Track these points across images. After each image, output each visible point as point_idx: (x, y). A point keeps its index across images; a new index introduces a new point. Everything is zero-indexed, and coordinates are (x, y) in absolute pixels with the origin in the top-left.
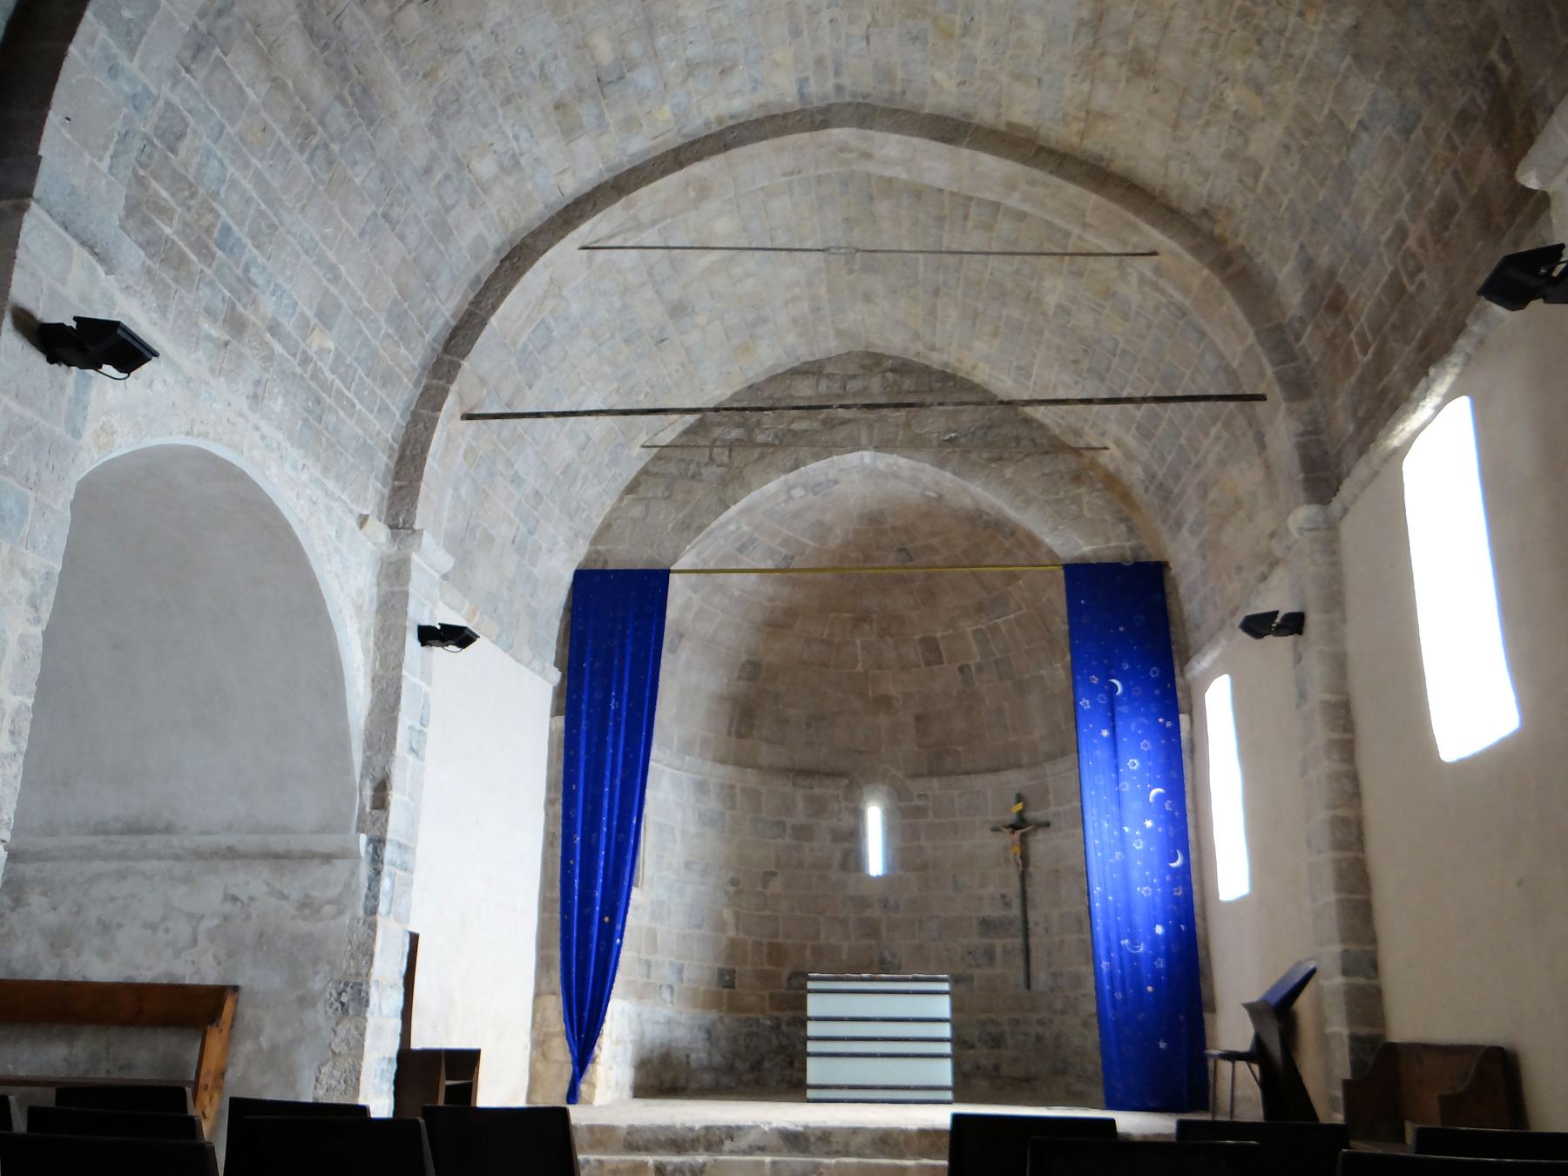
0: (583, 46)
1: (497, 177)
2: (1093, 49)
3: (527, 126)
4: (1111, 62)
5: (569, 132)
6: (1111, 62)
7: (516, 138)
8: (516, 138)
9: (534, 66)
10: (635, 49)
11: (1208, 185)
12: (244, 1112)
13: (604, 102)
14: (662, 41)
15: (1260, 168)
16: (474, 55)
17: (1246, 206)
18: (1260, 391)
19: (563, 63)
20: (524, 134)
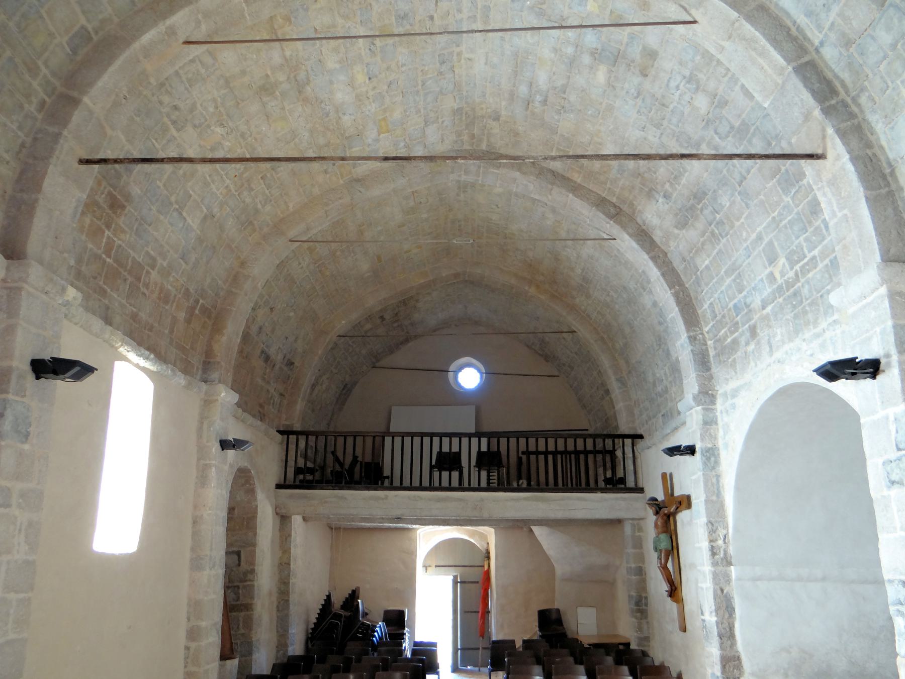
0: (610, 85)
1: (704, 90)
2: (295, 77)
3: (667, 85)
4: (281, 77)
5: (651, 55)
6: (281, 77)
7: (677, 88)
8: (677, 88)
9: (639, 101)
10: (587, 59)
11: (184, 79)
12: (342, 607)
13: (622, 48)
14: (570, 50)
15: (178, 130)
16: (658, 135)
17: (161, 103)
18: (84, 167)
19: (626, 86)
20: (673, 84)
